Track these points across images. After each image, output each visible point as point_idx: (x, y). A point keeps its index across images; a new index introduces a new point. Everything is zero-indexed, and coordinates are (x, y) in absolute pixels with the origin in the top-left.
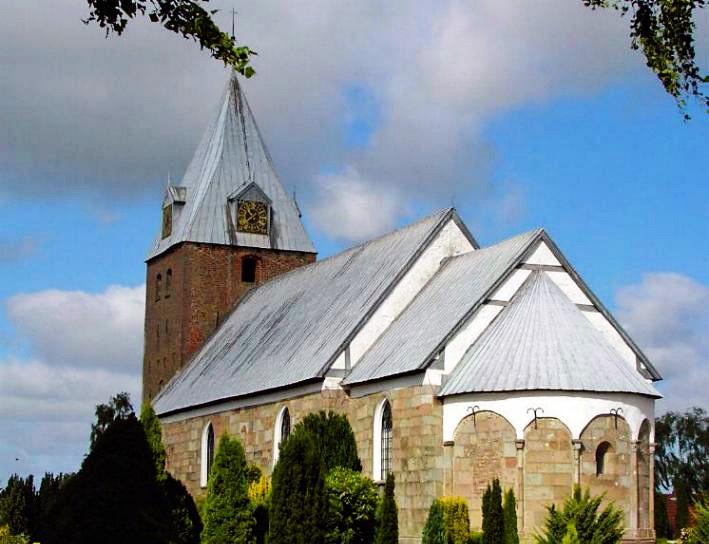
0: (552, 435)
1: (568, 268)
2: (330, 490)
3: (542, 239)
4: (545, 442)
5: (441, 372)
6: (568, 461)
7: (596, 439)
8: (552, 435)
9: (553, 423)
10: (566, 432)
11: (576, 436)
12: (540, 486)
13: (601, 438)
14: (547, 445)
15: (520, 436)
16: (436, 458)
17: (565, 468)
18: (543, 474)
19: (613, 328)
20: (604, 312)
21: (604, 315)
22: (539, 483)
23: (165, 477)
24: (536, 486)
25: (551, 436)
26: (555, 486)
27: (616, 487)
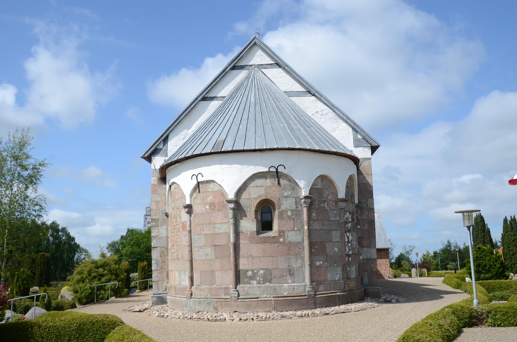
0: (211, 197)
1: (313, 92)
2: (401, 264)
4: (206, 204)
7: (251, 200)
8: (211, 197)
9: (212, 185)
10: (222, 193)
11: (231, 196)
12: (203, 246)
14: (208, 207)
15: (188, 202)
18: (206, 235)
19: (327, 108)
20: (323, 99)
21: (317, 97)
22: (202, 244)
23: (507, 274)
24: (201, 247)
25: (210, 199)
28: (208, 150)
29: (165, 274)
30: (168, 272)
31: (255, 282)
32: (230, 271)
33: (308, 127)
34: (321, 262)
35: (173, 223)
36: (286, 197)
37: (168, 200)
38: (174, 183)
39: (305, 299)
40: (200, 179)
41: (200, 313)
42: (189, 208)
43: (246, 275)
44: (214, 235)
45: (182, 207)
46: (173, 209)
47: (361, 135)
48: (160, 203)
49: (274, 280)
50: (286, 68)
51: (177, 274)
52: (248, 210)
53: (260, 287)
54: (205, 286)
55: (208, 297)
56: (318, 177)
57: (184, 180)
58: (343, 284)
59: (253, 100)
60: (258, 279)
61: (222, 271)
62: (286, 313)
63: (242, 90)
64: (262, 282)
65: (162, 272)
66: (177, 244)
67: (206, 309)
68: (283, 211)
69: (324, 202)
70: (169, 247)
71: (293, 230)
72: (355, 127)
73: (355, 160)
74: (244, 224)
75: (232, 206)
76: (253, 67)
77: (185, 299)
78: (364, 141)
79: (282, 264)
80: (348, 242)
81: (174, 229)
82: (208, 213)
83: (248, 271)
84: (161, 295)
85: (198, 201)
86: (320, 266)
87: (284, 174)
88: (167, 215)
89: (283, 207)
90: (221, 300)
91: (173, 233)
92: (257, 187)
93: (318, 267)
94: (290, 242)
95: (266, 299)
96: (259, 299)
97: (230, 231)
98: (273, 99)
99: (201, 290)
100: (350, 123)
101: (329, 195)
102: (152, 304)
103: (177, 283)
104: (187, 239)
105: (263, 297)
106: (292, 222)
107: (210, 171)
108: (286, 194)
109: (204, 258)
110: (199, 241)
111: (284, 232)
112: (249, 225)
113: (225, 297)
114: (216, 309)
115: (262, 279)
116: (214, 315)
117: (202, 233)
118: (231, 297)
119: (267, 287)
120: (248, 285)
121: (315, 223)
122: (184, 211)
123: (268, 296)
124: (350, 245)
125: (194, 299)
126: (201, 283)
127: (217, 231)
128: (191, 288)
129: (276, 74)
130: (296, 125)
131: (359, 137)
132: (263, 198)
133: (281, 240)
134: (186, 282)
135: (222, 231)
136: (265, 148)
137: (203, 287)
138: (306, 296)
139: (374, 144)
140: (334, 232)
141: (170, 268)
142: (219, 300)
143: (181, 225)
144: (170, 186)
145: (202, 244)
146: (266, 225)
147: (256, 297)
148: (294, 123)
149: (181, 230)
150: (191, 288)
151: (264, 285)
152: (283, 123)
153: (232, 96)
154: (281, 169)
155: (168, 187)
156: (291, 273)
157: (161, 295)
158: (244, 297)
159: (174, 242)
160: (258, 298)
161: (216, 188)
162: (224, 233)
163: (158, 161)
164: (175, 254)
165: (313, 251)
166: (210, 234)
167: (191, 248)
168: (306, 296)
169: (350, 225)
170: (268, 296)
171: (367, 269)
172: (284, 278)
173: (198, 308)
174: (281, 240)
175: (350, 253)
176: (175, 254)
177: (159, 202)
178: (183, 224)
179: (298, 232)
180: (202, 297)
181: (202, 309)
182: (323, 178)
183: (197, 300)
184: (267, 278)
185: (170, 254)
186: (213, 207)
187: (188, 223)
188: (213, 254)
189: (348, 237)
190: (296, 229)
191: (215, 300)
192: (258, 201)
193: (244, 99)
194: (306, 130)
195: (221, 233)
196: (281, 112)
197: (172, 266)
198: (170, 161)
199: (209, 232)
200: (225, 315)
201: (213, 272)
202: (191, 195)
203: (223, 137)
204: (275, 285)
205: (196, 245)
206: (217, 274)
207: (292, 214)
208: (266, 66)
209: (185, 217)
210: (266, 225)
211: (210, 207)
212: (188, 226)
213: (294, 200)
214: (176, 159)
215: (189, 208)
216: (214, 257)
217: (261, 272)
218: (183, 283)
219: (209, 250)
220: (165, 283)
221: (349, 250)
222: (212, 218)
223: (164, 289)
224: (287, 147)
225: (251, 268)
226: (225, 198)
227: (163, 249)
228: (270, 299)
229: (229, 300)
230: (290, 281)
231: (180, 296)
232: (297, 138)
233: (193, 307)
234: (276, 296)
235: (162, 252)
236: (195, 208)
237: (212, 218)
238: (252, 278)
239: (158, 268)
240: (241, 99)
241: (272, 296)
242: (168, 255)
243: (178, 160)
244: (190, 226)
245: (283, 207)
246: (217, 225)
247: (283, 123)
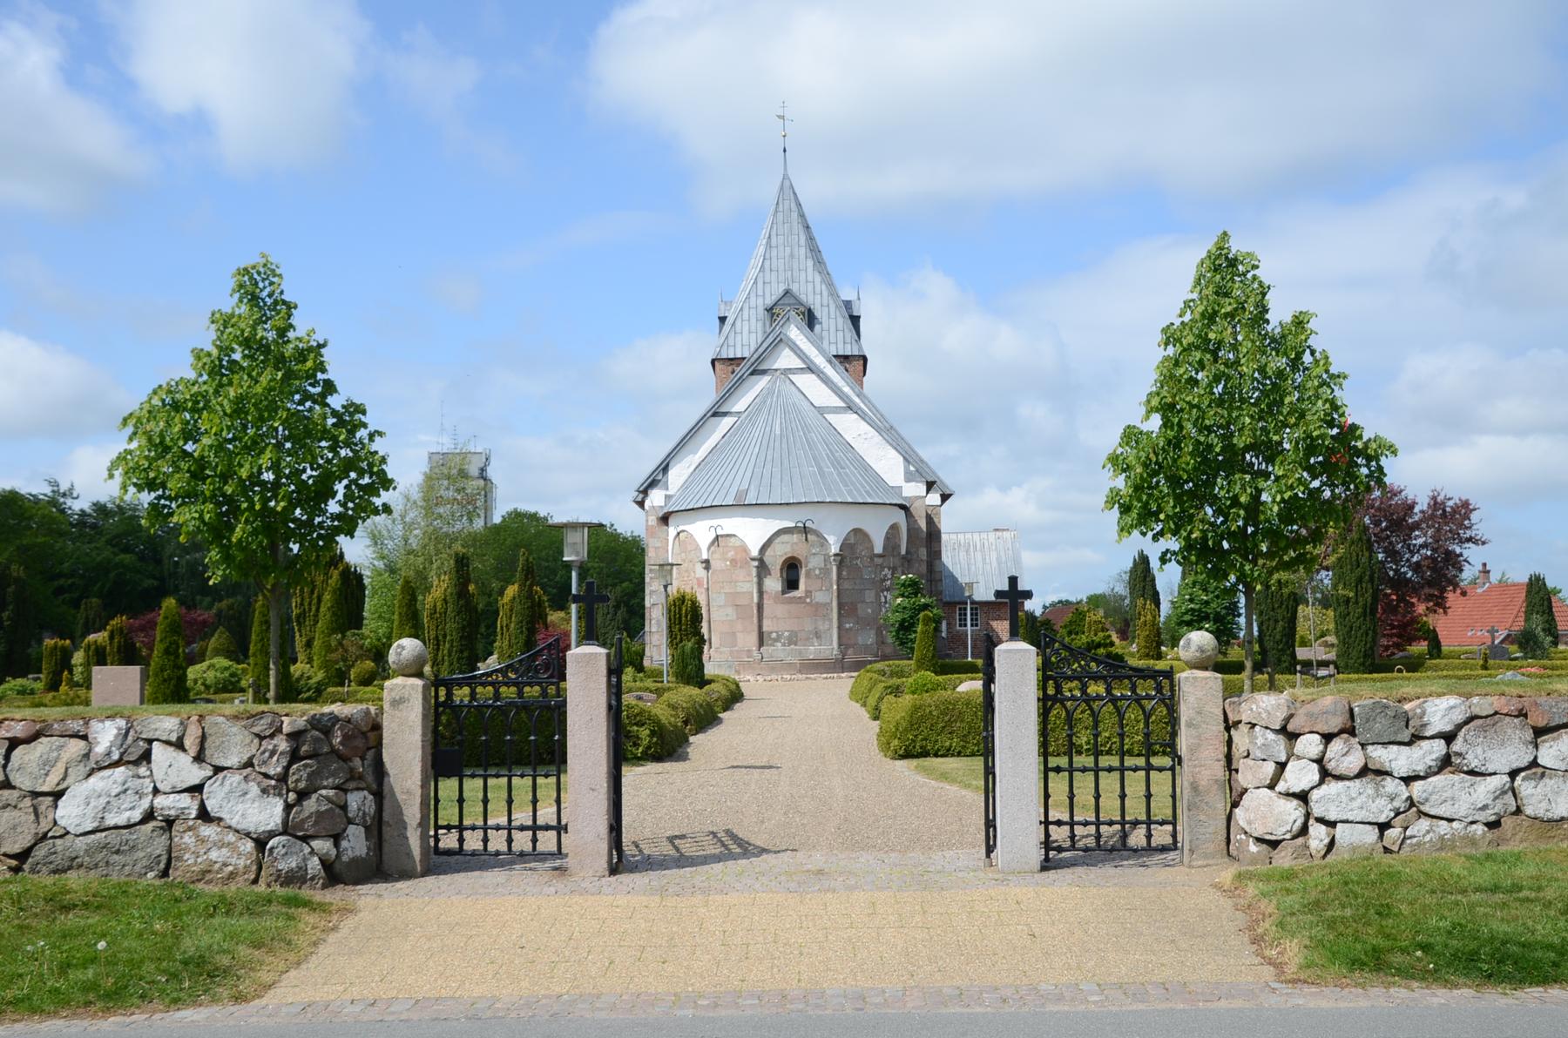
10: (744, 549)
11: (755, 553)
15: (705, 557)
25: (731, 554)
42: (707, 564)
85: (717, 556)
89: (810, 566)
105: (789, 659)
112: (774, 584)
146: (791, 584)
161: (738, 543)
201: (734, 634)
210: (791, 584)
215: (707, 564)
219: (730, 611)
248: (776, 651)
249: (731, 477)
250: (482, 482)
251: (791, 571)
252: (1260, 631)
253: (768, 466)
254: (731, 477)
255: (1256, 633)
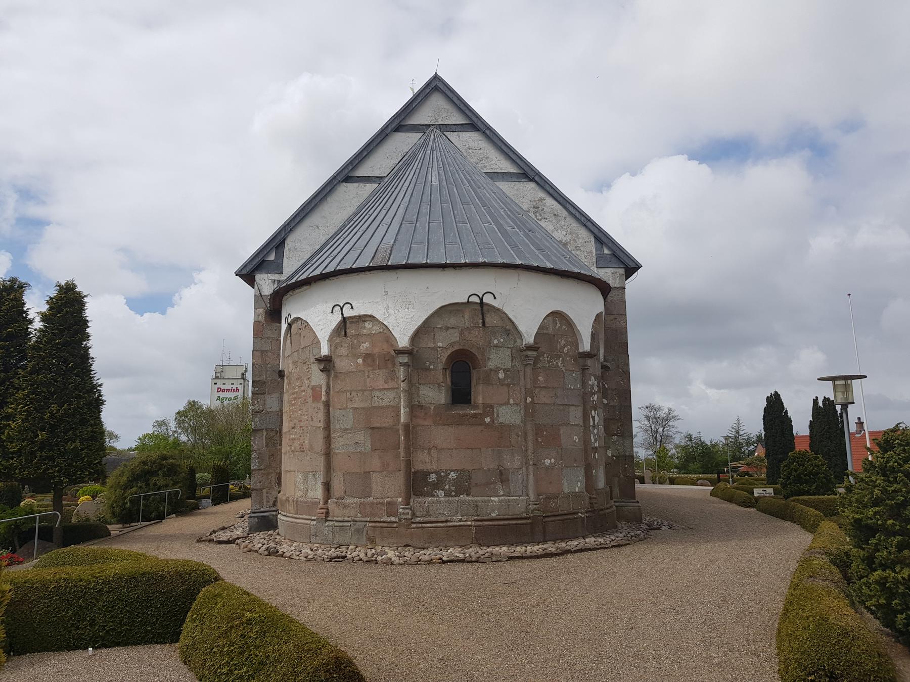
0: (367, 344)
3: (436, 89)
4: (357, 356)
5: (276, 277)
6: (392, 385)
7: (445, 342)
8: (367, 344)
9: (368, 325)
10: (386, 335)
11: (403, 341)
13: (452, 345)
14: (360, 361)
15: (325, 351)
16: (267, 397)
17: (388, 398)
20: (537, 178)
24: (346, 430)
25: (365, 346)
26: (373, 428)
27: (487, 425)
28: (364, 262)
29: (273, 477)
30: (280, 473)
31: (441, 493)
32: (398, 474)
33: (530, 231)
34: (553, 460)
35: (294, 388)
36: (496, 346)
37: (284, 349)
38: (298, 319)
39: (527, 524)
40: (348, 313)
41: (343, 549)
42: (326, 363)
43: (425, 479)
44: (370, 411)
45: (312, 359)
46: (295, 363)
47: (609, 248)
48: (269, 354)
49: (473, 490)
50: (487, 132)
51: (300, 477)
52: (432, 367)
53: (450, 502)
54: (352, 500)
55: (357, 519)
56: (548, 315)
57: (318, 314)
58: (587, 499)
59: (435, 180)
60: (447, 487)
61: (384, 473)
62: (497, 549)
63: (416, 165)
64: (453, 493)
65: (268, 474)
66: (302, 424)
67: (354, 540)
68: (491, 370)
69: (558, 357)
70: (285, 429)
71: (507, 403)
72: (600, 235)
73: (604, 288)
74: (425, 392)
75: (404, 359)
76: (431, 128)
77: (315, 523)
78: (613, 259)
79: (488, 463)
80: (594, 426)
81: (295, 399)
82: (360, 371)
83: (429, 473)
84: (265, 514)
85: (343, 351)
86: (552, 467)
87: (494, 307)
88: (281, 374)
89: (492, 364)
90: (381, 524)
91: (294, 405)
92: (447, 328)
93: (547, 468)
94: (502, 425)
95: (462, 523)
96: (449, 524)
97: (399, 402)
98: (469, 182)
99: (344, 506)
100: (592, 228)
101: (565, 346)
102: (250, 529)
103: (298, 494)
104: (321, 415)
105: (458, 519)
106: (506, 388)
107: (368, 300)
108: (496, 342)
109: (352, 450)
110: (343, 419)
111: (491, 406)
112: (435, 395)
113: (386, 519)
114: (372, 540)
115: (453, 488)
116: (370, 553)
117: (350, 405)
118: (400, 520)
119: (463, 502)
120: (430, 499)
121: (543, 393)
122: (315, 369)
123: (465, 518)
124: (596, 431)
125: (331, 523)
126: (345, 493)
127: (376, 402)
128: (326, 502)
129: (469, 140)
130: (510, 226)
131: (606, 251)
132: (456, 348)
133: (488, 420)
134: (318, 493)
135: (386, 402)
136: (463, 261)
137: (349, 501)
138: (529, 518)
139: (632, 265)
140: (573, 408)
141: (285, 466)
142: (378, 524)
143: (310, 391)
144: (290, 325)
145: (350, 425)
146: (461, 395)
147: (443, 519)
148: (507, 222)
149: (310, 400)
150: (326, 502)
151: (457, 499)
152: (489, 223)
153: (397, 173)
154: (488, 299)
155: (284, 326)
156: (503, 476)
157: (265, 514)
158: (422, 520)
159: (295, 421)
160: (447, 521)
161: (377, 329)
162: (389, 407)
163: (267, 283)
164: (297, 444)
165: (540, 440)
166: (363, 408)
167: (330, 431)
168: (529, 518)
169: (595, 398)
170: (465, 518)
171: (624, 470)
172: (492, 486)
173: (339, 539)
174: (488, 420)
175: (597, 445)
176: (297, 444)
177: (267, 351)
178: (315, 390)
179: (515, 407)
180: (346, 519)
181: (347, 541)
182: (557, 316)
183: (337, 524)
184: (463, 486)
185: (285, 442)
186: (369, 361)
187: (324, 389)
188: (368, 444)
189: (593, 418)
190: (511, 401)
191: (371, 525)
192: (449, 352)
193: (421, 180)
194: (527, 236)
195: (384, 407)
196: (485, 205)
197: (288, 463)
198: (293, 281)
199: (362, 405)
200: (391, 554)
201: (367, 475)
202: (331, 340)
203: (390, 239)
204: (476, 498)
205: (338, 427)
206: (376, 478)
207: (506, 377)
208: (454, 128)
209: (318, 378)
210: (461, 395)
211: (364, 360)
212: (324, 393)
213: (508, 352)
214: (304, 276)
215: (326, 363)
216: (369, 448)
217: (453, 475)
218: (311, 494)
219: (362, 437)
220: (274, 493)
221: (596, 440)
222: (368, 380)
223: (271, 503)
224: (500, 261)
225: (435, 467)
226: (392, 345)
227: (272, 434)
228: (469, 523)
229: (395, 525)
230: (502, 493)
231: (305, 517)
232: (514, 246)
233: (331, 537)
234: (479, 518)
235: (269, 439)
236: (341, 364)
237: (368, 380)
238: (438, 485)
239: (262, 467)
240: (414, 180)
241: (471, 518)
242: (280, 444)
243: (308, 278)
244: (328, 393)
245: (492, 364)
246: (377, 393)
247: (489, 223)
248: (438, 505)
249: (362, 242)
250: (242, 381)
251: (462, 372)
252: (608, 481)
253: (424, 219)
254: (362, 242)
255: (601, 484)
